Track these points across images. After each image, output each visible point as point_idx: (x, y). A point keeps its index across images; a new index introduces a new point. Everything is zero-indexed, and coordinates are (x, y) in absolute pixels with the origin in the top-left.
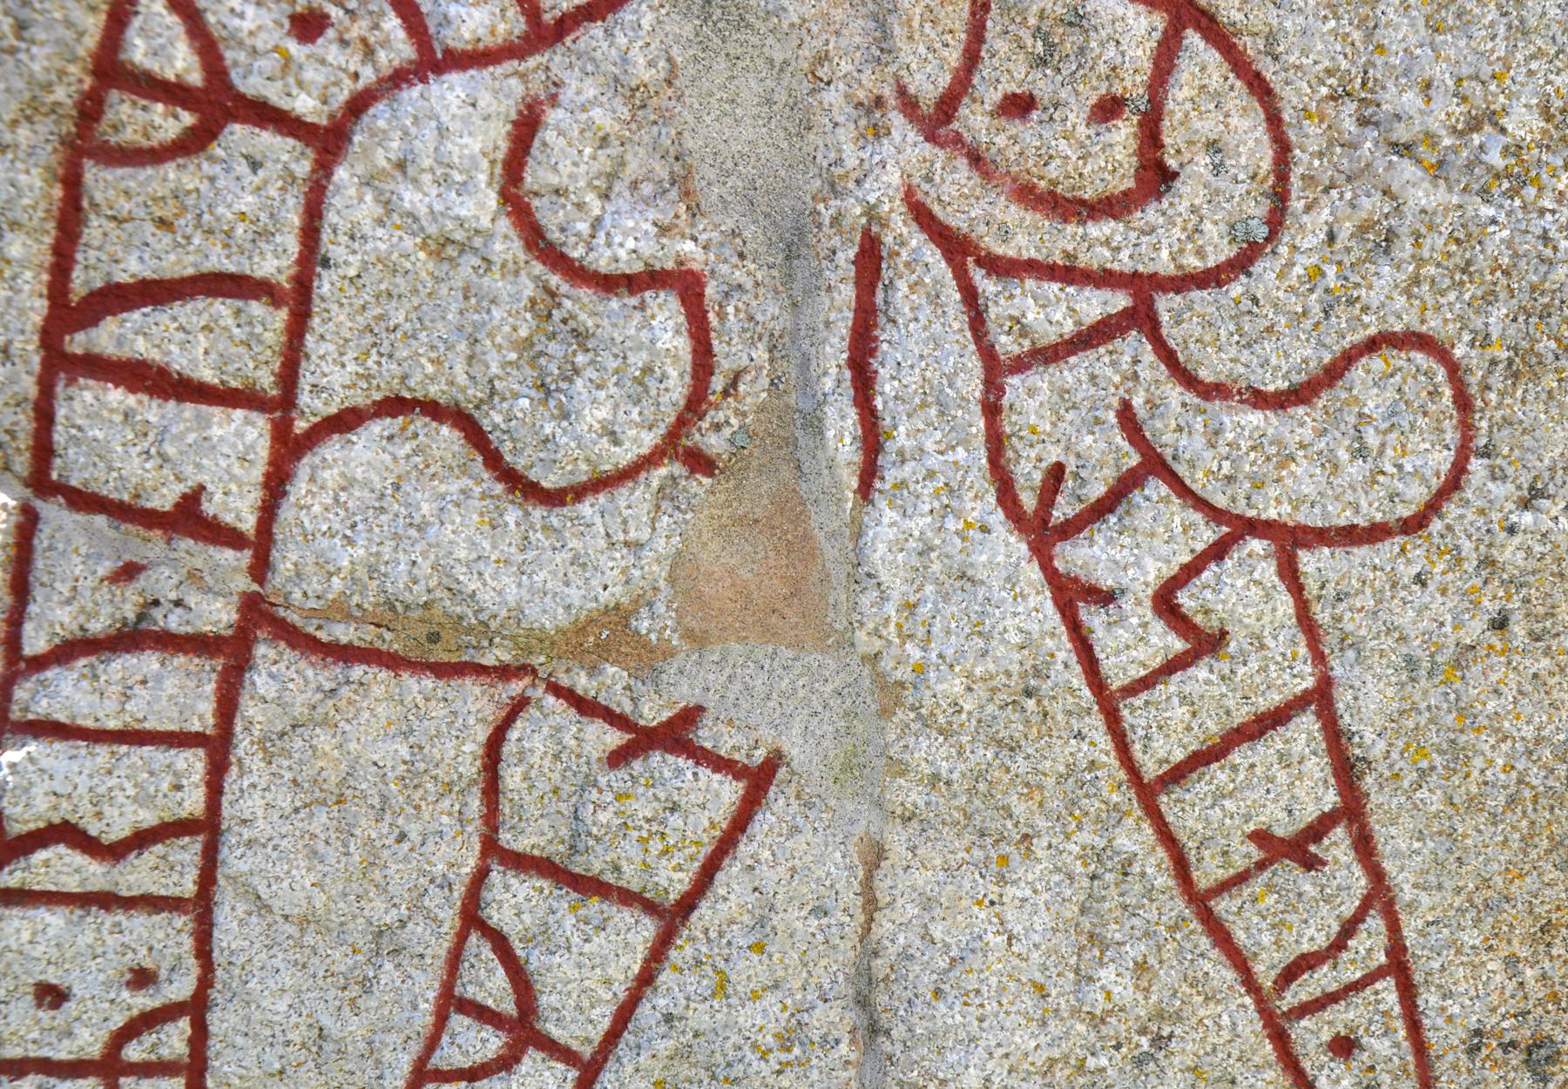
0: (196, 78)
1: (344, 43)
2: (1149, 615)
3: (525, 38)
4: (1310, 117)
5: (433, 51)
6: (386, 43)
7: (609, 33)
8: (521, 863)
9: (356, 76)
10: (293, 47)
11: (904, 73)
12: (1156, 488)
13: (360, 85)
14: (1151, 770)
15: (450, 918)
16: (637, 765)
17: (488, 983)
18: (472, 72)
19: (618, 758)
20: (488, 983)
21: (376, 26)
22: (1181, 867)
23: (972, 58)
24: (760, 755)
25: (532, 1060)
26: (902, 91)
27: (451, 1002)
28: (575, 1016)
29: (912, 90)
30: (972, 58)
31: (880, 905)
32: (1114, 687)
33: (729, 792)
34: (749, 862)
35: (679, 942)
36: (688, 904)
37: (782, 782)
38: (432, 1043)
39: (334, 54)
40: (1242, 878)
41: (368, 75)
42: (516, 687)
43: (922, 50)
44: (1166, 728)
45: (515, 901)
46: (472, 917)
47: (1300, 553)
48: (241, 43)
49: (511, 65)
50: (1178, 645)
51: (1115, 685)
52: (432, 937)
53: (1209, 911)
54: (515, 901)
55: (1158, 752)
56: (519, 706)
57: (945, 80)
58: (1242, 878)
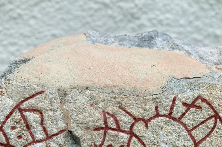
0: (6, 143)
1: (24, 139)
3: (46, 138)
4: (118, 39)
5: (35, 140)
6: (29, 139)
7: (57, 138)
9: (25, 143)
10: (17, 139)
11: (95, 142)
12: (45, 137)
13: (26, 144)
18: (40, 143)
21: (28, 137)
23: (104, 140)
26: (95, 144)
29: (96, 144)
30: (104, 140)
39: (23, 141)
40: (184, 114)
41: (27, 143)
43: (97, 139)
48: (11, 139)
49: (45, 142)
57: (100, 143)
58: (184, 114)
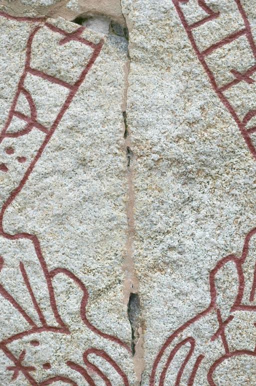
2: (198, 6)
8: (35, 72)
14: (201, 49)
15: (15, 85)
16: (67, 44)
17: (23, 106)
19: (62, 42)
20: (23, 106)
22: (212, 80)
24: (98, 41)
25: (34, 130)
27: (13, 112)
28: (46, 117)
31: (130, 85)
32: (46, 134)
33: (90, 50)
34: (95, 71)
35: (75, 95)
36: (78, 83)
37: (104, 48)
38: (8, 124)
42: (37, 24)
44: (206, 34)
45: (32, 82)
46: (21, 89)
47: (27, 123)
50: (206, 14)
51: (45, 134)
52: (9, 91)
53: (222, 94)
54: (32, 82)
55: (204, 43)
56: (38, 28)
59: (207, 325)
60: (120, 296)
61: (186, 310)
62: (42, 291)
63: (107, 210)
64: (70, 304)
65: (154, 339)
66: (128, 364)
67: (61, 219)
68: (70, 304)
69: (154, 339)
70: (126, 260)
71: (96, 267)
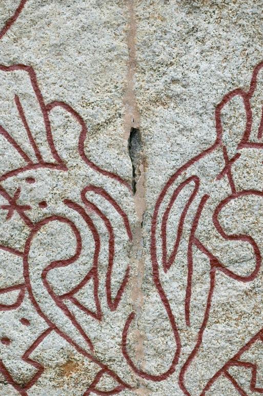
59: (212, 163)
60: (120, 131)
61: (190, 148)
62: (37, 124)
63: (107, 40)
64: (68, 138)
65: (156, 177)
66: (129, 203)
67: (59, 49)
68: (68, 138)
69: (156, 177)
70: (127, 93)
71: (95, 98)
